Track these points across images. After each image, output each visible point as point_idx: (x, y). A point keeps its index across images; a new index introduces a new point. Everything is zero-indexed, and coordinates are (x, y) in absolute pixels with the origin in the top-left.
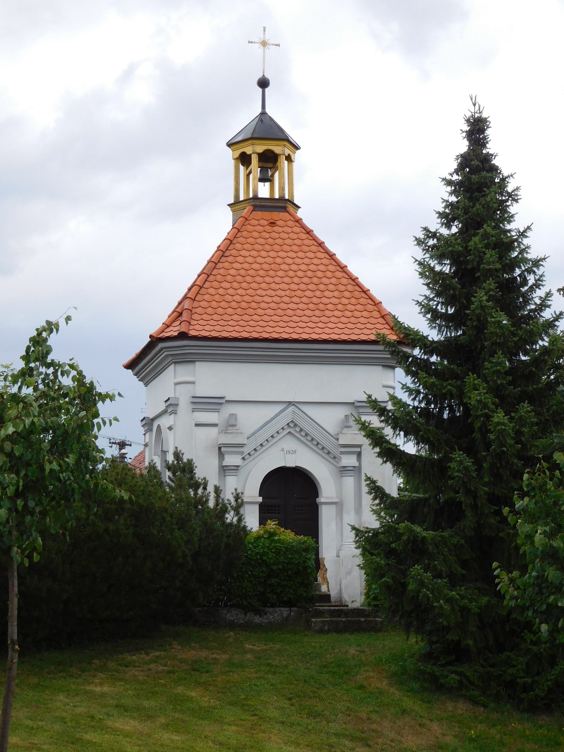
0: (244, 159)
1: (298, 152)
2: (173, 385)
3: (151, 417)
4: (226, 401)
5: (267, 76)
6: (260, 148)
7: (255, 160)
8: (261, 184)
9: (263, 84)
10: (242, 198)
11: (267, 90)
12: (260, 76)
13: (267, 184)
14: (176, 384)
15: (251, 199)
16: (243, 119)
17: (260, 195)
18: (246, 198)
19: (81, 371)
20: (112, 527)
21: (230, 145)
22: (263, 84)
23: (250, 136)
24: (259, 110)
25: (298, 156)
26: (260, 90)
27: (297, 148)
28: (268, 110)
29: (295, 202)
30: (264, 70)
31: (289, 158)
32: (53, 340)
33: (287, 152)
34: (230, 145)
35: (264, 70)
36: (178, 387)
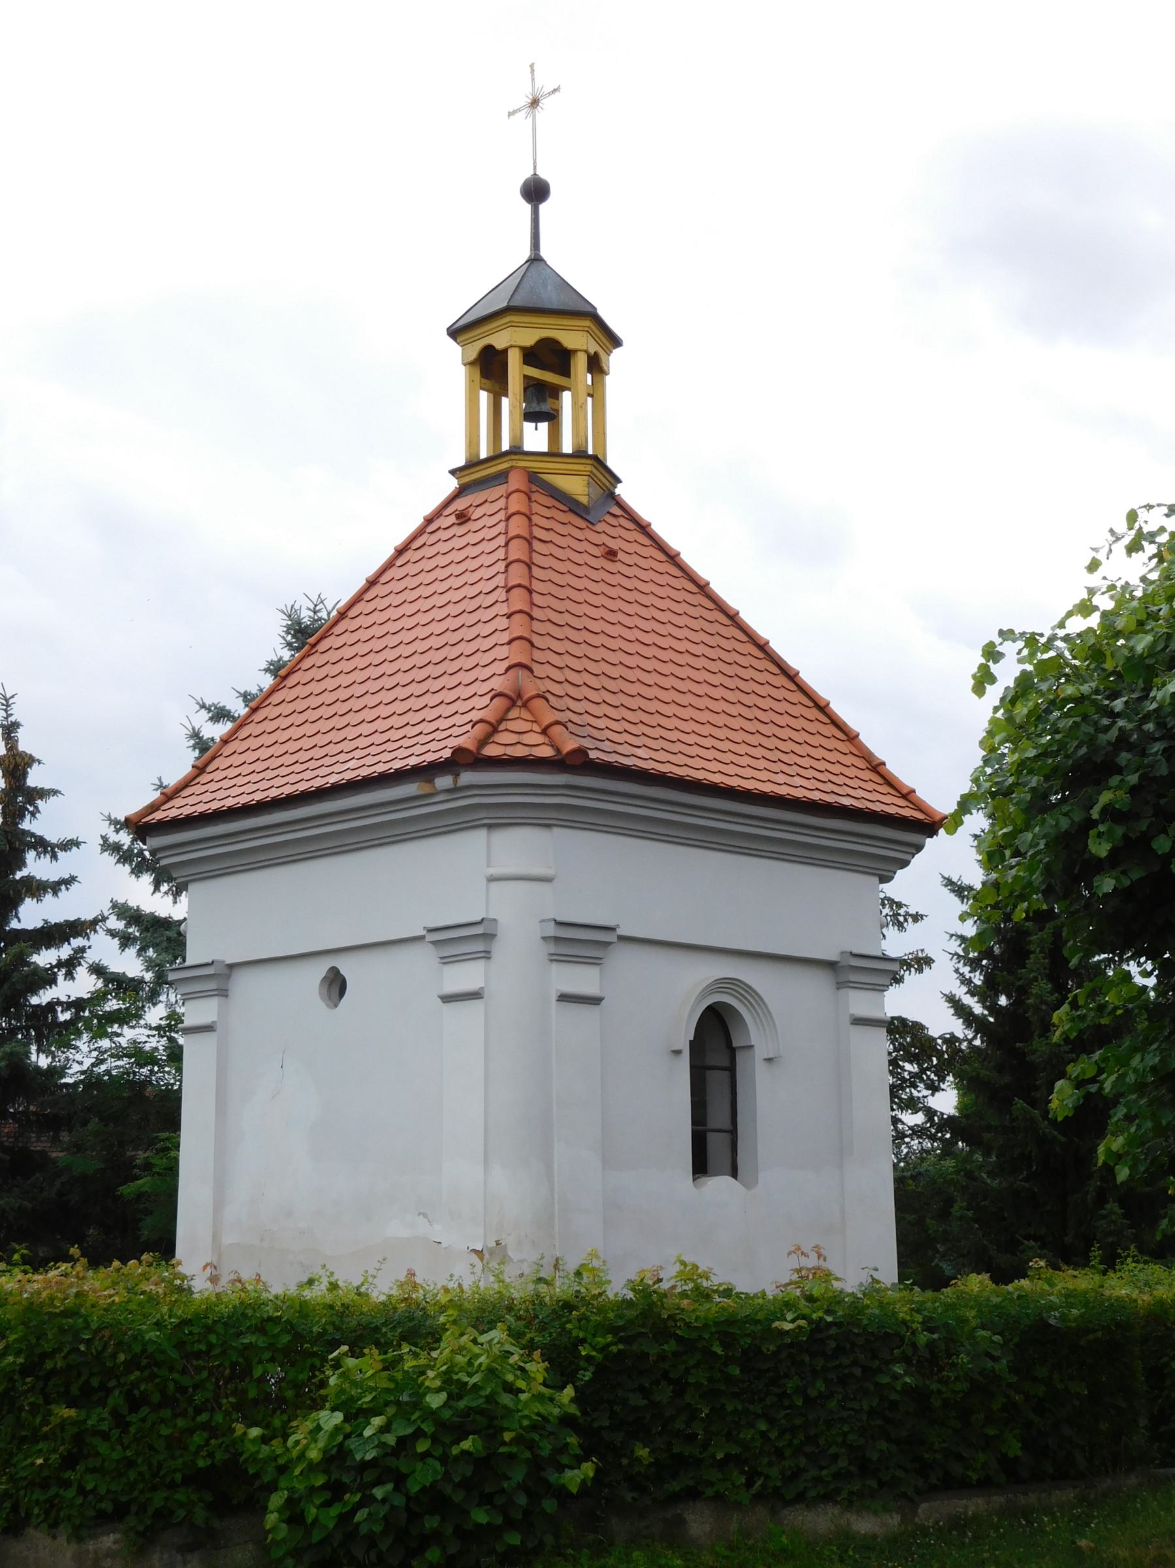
0: (489, 367)
1: (616, 352)
2: (485, 881)
3: (229, 961)
4: (622, 938)
5: (543, 174)
6: (529, 338)
7: (514, 360)
8: (528, 427)
9: (536, 192)
10: (483, 455)
11: (543, 207)
12: (528, 174)
13: (544, 426)
14: (492, 879)
15: (506, 453)
16: (483, 269)
17: (527, 447)
18: (491, 454)
19: (1024, 633)
20: (65, 1137)
21: (455, 332)
22: (536, 192)
23: (505, 304)
24: (525, 253)
25: (616, 360)
26: (527, 207)
27: (616, 342)
28: (544, 253)
29: (610, 464)
30: (535, 162)
31: (596, 366)
32: (35, 765)
33: (593, 348)
34: (455, 332)
35: (535, 162)
36: (494, 885)
